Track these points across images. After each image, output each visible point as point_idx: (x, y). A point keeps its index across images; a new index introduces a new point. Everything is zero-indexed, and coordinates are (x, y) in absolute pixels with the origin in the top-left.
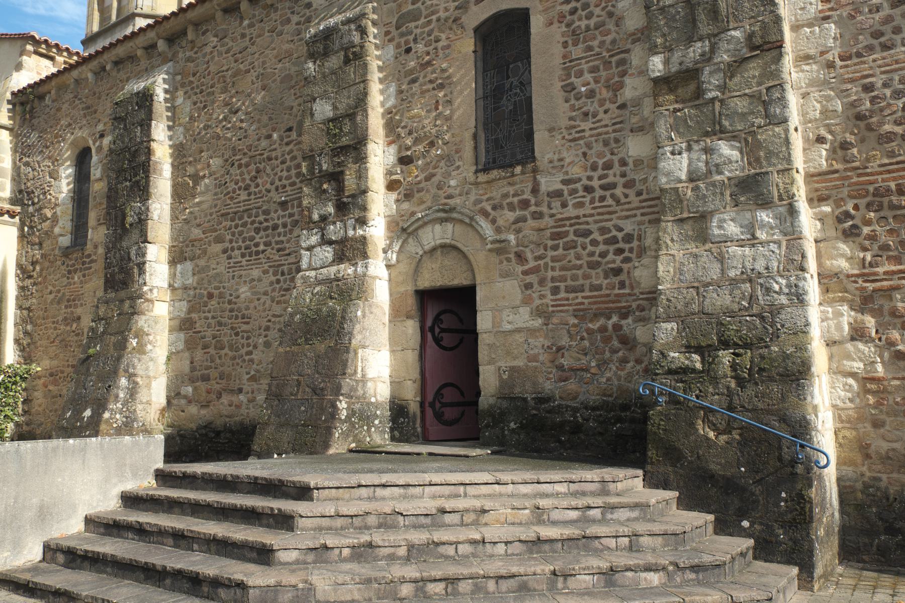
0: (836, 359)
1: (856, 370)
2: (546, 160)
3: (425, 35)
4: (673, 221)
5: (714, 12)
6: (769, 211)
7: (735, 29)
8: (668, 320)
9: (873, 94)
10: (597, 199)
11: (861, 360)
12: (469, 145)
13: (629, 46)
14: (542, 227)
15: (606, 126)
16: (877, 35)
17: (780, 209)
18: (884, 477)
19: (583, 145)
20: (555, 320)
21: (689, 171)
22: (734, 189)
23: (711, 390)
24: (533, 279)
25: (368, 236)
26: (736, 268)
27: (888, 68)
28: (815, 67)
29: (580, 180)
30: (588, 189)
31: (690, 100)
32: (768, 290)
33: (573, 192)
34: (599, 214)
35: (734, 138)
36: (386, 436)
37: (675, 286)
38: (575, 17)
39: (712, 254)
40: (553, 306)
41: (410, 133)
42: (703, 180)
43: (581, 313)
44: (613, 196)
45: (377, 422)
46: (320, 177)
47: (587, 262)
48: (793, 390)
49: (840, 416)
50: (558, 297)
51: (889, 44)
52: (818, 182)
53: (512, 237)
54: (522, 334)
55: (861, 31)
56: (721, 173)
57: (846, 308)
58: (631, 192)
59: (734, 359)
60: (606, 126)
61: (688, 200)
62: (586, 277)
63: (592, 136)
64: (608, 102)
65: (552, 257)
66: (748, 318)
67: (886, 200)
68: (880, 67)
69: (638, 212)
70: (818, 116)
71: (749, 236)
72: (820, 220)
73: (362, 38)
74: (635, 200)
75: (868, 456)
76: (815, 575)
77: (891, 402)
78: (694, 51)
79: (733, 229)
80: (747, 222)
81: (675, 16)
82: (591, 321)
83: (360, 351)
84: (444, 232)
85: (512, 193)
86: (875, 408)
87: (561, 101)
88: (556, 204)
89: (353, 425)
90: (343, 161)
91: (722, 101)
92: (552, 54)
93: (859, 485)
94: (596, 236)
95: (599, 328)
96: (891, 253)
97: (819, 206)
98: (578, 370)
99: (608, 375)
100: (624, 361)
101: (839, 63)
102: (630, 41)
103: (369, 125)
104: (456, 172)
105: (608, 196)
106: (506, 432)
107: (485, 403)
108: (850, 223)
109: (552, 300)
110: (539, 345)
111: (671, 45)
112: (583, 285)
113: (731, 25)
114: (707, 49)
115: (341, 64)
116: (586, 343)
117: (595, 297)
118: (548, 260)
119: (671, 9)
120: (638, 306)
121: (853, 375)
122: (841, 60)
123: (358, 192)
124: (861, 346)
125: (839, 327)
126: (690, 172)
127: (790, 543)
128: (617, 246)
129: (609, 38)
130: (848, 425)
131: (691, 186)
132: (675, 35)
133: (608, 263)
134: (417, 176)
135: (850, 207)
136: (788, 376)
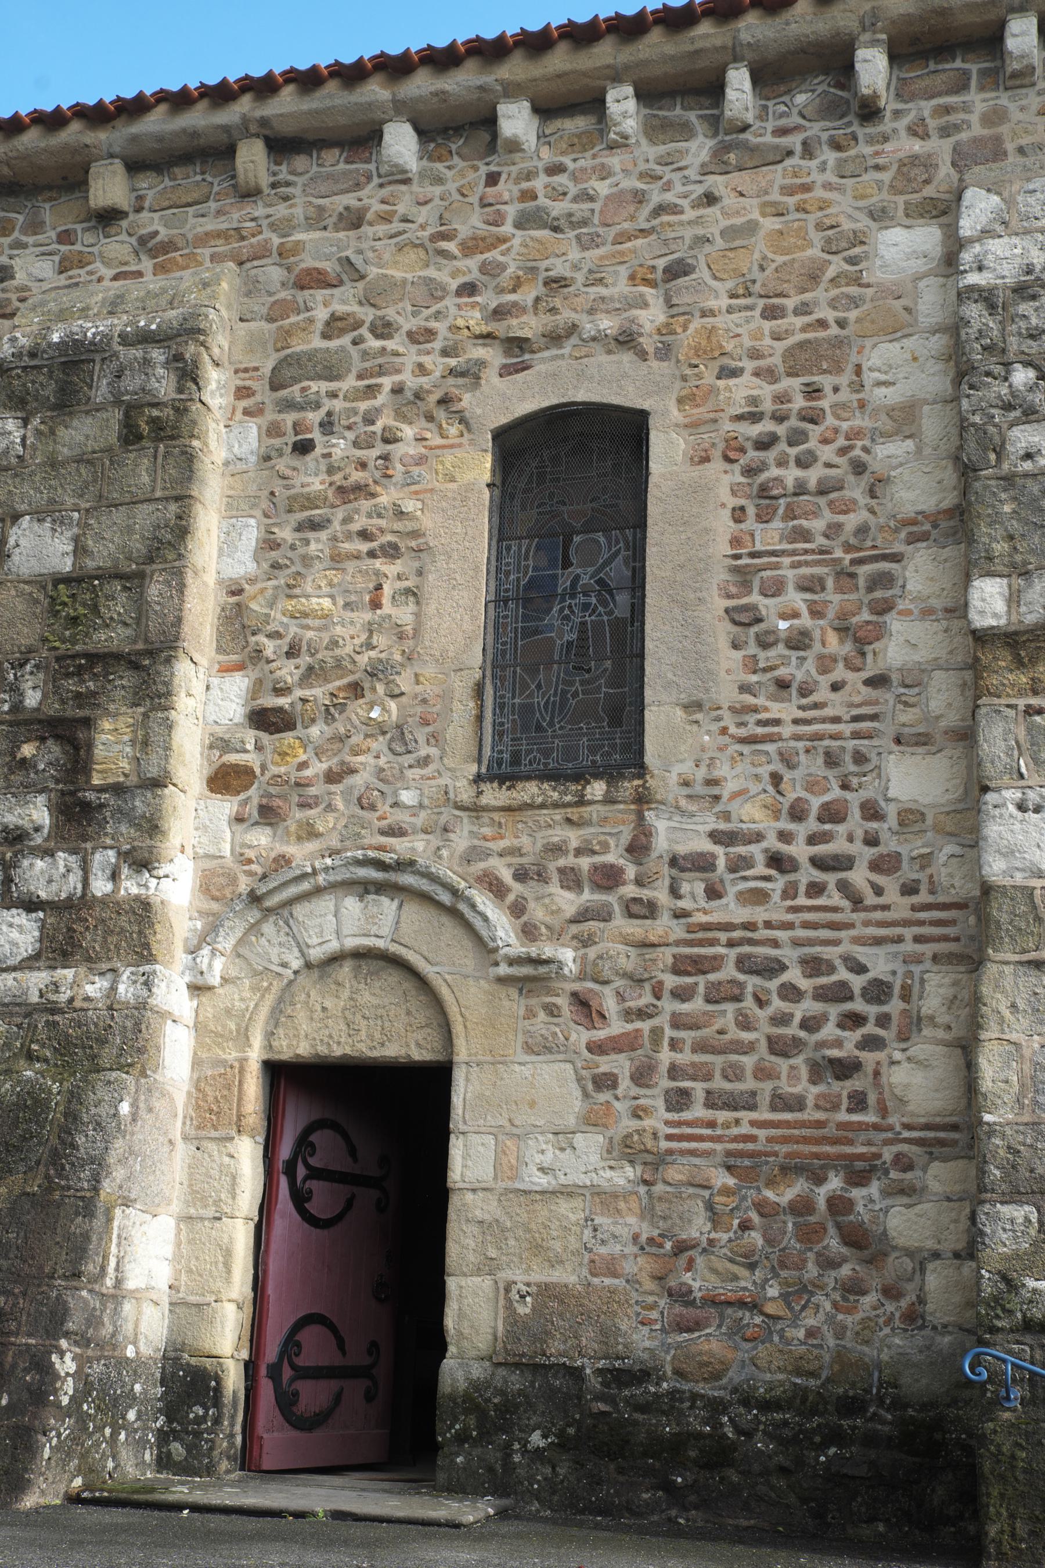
2: (673, 778)
3: (358, 419)
8: (1014, 1196)
10: (802, 889)
12: (463, 709)
13: (898, 547)
14: (653, 939)
15: (836, 720)
19: (775, 757)
20: (674, 1173)
24: (620, 1065)
25: (155, 900)
29: (759, 837)
30: (777, 862)
33: (737, 865)
34: (806, 925)
36: (147, 1457)
37: (1026, 1118)
38: (771, 455)
40: (669, 1138)
41: (292, 652)
43: (747, 1162)
44: (844, 887)
45: (131, 1415)
46: (11, 724)
47: (769, 1038)
50: (686, 1115)
53: (567, 955)
54: (578, 1202)
58: (890, 884)
60: (836, 720)
62: (762, 1073)
63: (797, 738)
64: (841, 665)
65: (674, 1015)
69: (908, 933)
73: (180, 390)
74: (901, 906)
82: (771, 1183)
83: (118, 1212)
84: (371, 919)
85: (574, 844)
87: (723, 643)
88: (694, 887)
89: (82, 1419)
90: (94, 694)
92: (707, 531)
94: (794, 975)
95: (791, 1202)
98: (729, 1304)
99: (811, 1322)
100: (853, 1289)
102: (903, 535)
103: (186, 613)
104: (417, 772)
105: (831, 886)
106: (517, 1458)
107: (460, 1375)
109: (667, 1123)
110: (625, 1233)
112: (753, 1094)
115: (113, 439)
116: (756, 1238)
117: (787, 1124)
118: (662, 1021)
119: (1029, 483)
120: (898, 1157)
123: (134, 780)
128: (848, 1006)
129: (851, 521)
133: (821, 1045)
134: (303, 766)
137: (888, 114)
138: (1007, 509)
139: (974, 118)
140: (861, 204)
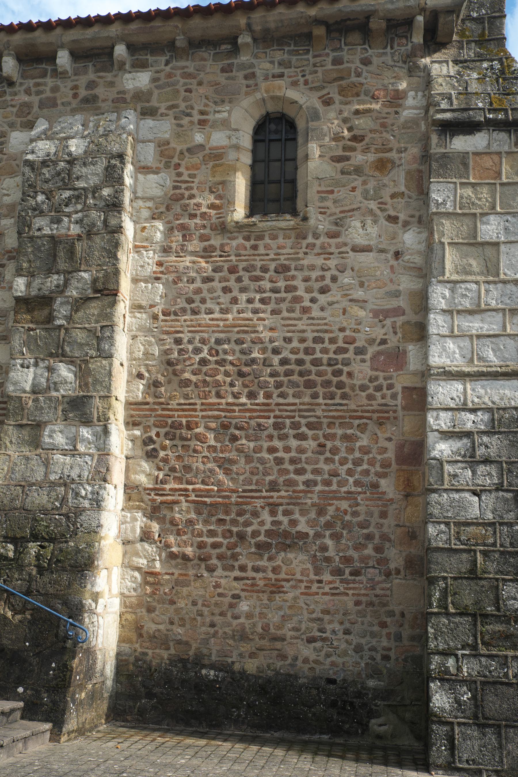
0: (128, 556)
1: (141, 566)
4: (14, 425)
5: (72, 253)
6: (89, 429)
7: (85, 271)
9: (180, 347)
11: (146, 558)
13: (4, 261)
16: (190, 301)
17: (97, 428)
18: (150, 652)
21: (33, 384)
22: (66, 406)
23: (16, 576)
26: (56, 473)
27: (193, 329)
28: (144, 316)
31: (42, 323)
32: (77, 494)
35: (72, 363)
37: (6, 483)
39: (41, 458)
42: (43, 393)
48: (78, 579)
49: (125, 602)
51: (196, 310)
52: (134, 410)
55: (180, 295)
56: (57, 390)
57: (140, 514)
59: (39, 551)
61: (28, 409)
66: (57, 517)
67: (178, 432)
68: (188, 326)
70: (141, 356)
71: (71, 447)
72: (132, 440)
75: (141, 635)
76: (64, 730)
77: (162, 592)
78: (51, 282)
79: (60, 440)
80: (72, 435)
81: (40, 247)
86: (150, 596)
91: (67, 329)
93: (132, 659)
96: (176, 474)
97: (132, 430)
101: (161, 317)
102: (6, 257)
108: (152, 447)
111: (34, 272)
113: (83, 267)
114: (61, 282)
119: (38, 240)
121: (138, 569)
122: (164, 315)
124: (146, 546)
125: (133, 530)
126: (34, 385)
127: (51, 704)
130: (130, 610)
131: (33, 397)
132: (38, 264)
135: (153, 434)
136: (76, 567)
137: (18, 84)
138: (30, 250)
139: (48, 89)
140: (5, 120)
